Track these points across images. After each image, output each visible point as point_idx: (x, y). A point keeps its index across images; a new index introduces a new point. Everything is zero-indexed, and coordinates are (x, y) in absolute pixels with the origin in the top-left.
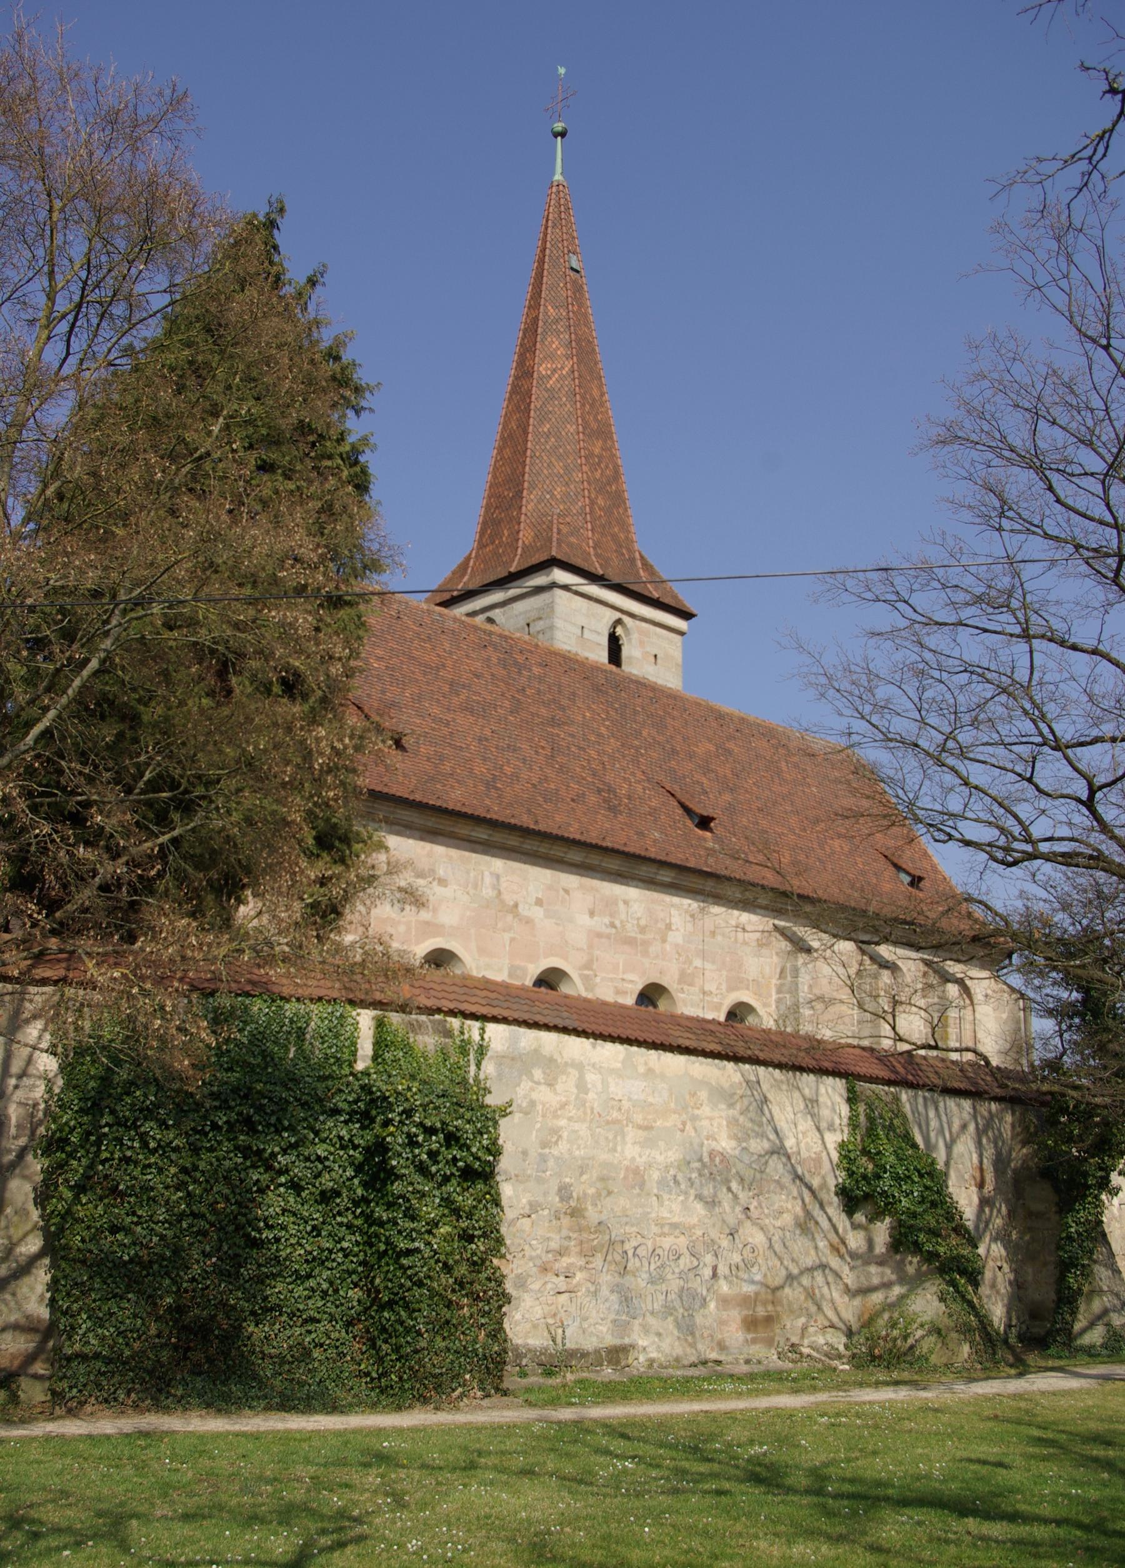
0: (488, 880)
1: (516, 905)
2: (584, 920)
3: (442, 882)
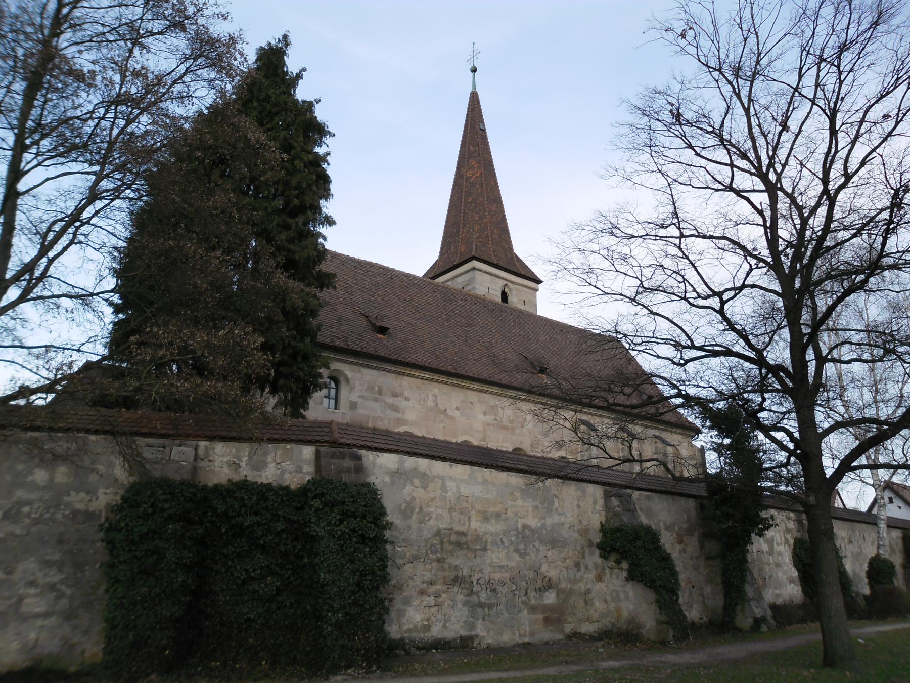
0: (431, 397)
1: (446, 410)
2: (481, 417)
3: (407, 399)
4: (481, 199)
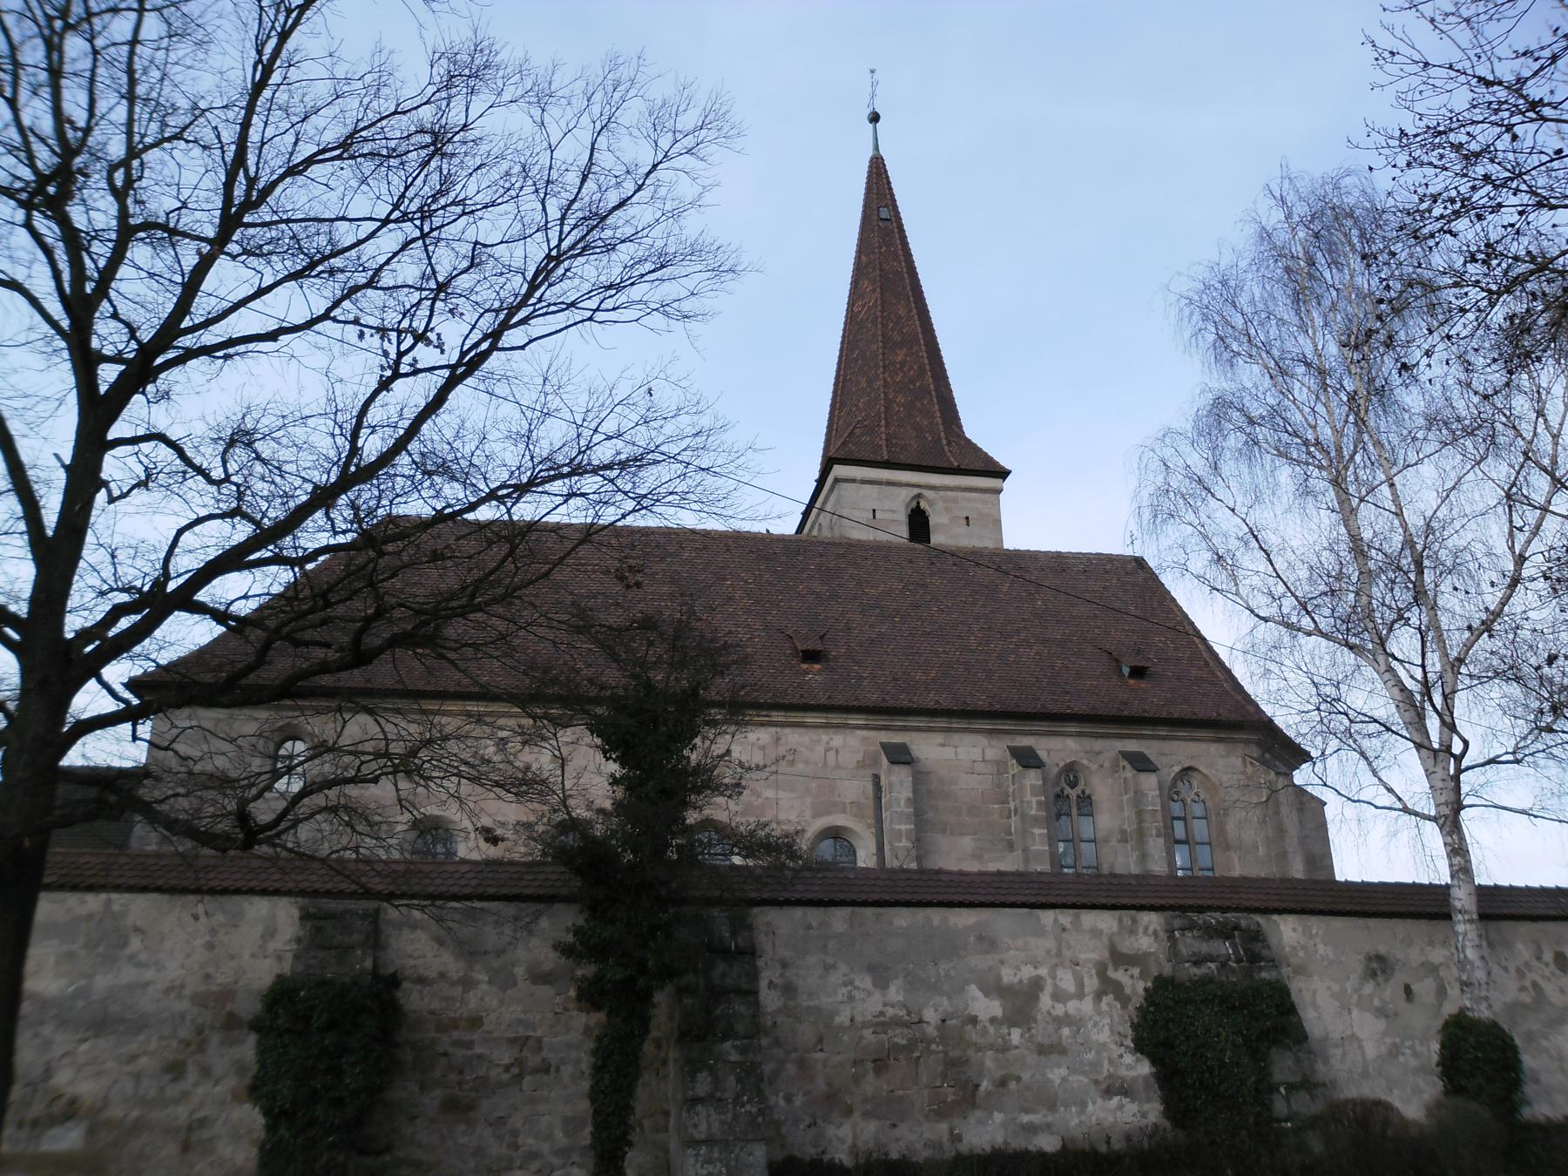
4: (874, 347)
